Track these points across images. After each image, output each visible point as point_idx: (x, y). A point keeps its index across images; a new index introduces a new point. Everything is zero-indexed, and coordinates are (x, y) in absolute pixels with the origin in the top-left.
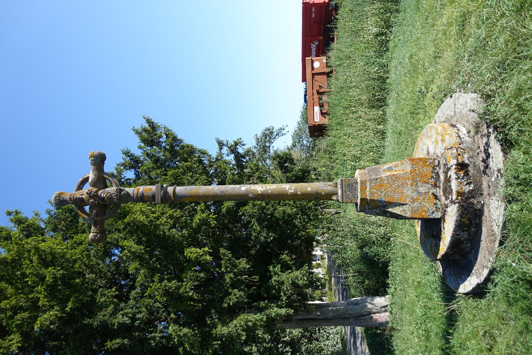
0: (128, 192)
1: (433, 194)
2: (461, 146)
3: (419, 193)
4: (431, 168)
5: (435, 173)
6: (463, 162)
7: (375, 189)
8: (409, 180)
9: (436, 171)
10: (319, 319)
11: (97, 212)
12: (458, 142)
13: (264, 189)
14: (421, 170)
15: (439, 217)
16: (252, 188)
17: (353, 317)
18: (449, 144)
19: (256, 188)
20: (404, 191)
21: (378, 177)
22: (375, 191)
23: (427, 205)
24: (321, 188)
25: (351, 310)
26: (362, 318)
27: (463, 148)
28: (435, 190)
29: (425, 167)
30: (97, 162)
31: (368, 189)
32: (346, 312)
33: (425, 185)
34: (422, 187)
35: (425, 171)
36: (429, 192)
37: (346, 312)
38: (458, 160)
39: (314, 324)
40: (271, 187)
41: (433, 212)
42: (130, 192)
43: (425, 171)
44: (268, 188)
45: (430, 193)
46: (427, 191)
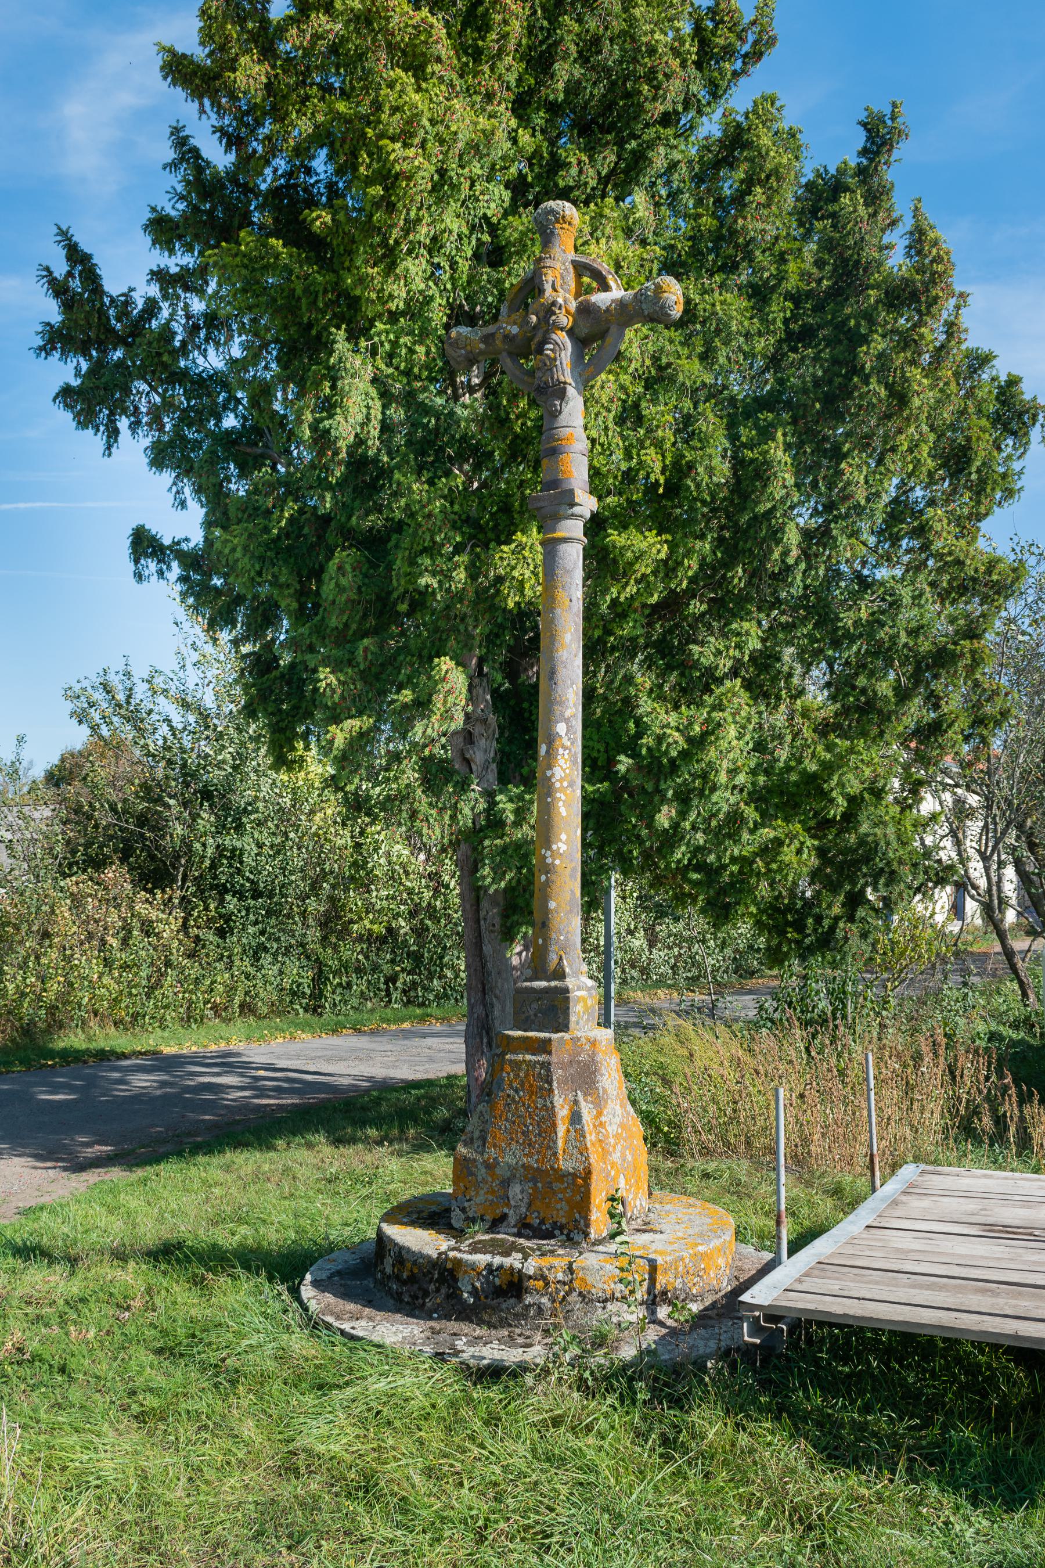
0: (560, 412)
1: (504, 1217)
2: (573, 1297)
3: (506, 1183)
4: (564, 1221)
5: (554, 1229)
6: (527, 1291)
7: (527, 1075)
8: (537, 1161)
9: (557, 1232)
10: (478, 921)
11: (515, 336)
12: (589, 1292)
13: (558, 785)
14: (560, 1196)
15: (453, 1222)
16: (561, 751)
17: (487, 1015)
18: (583, 1269)
19: (561, 762)
20: (514, 1145)
21: (555, 1084)
22: (522, 1074)
23: (478, 1200)
24: (554, 936)
25: (503, 1011)
26: (485, 1040)
27: (569, 1299)
28: (513, 1223)
29: (567, 1208)
30: (644, 306)
31: (528, 1057)
32: (497, 997)
33: (526, 1200)
34: (522, 1192)
35: (559, 1206)
36: (508, 1205)
37: (497, 997)
38: (530, 1277)
39: (468, 906)
40: (561, 804)
41: (463, 1210)
42: (561, 417)
43: (559, 1206)
44: (558, 795)
45: (506, 1210)
46: (512, 1203)
